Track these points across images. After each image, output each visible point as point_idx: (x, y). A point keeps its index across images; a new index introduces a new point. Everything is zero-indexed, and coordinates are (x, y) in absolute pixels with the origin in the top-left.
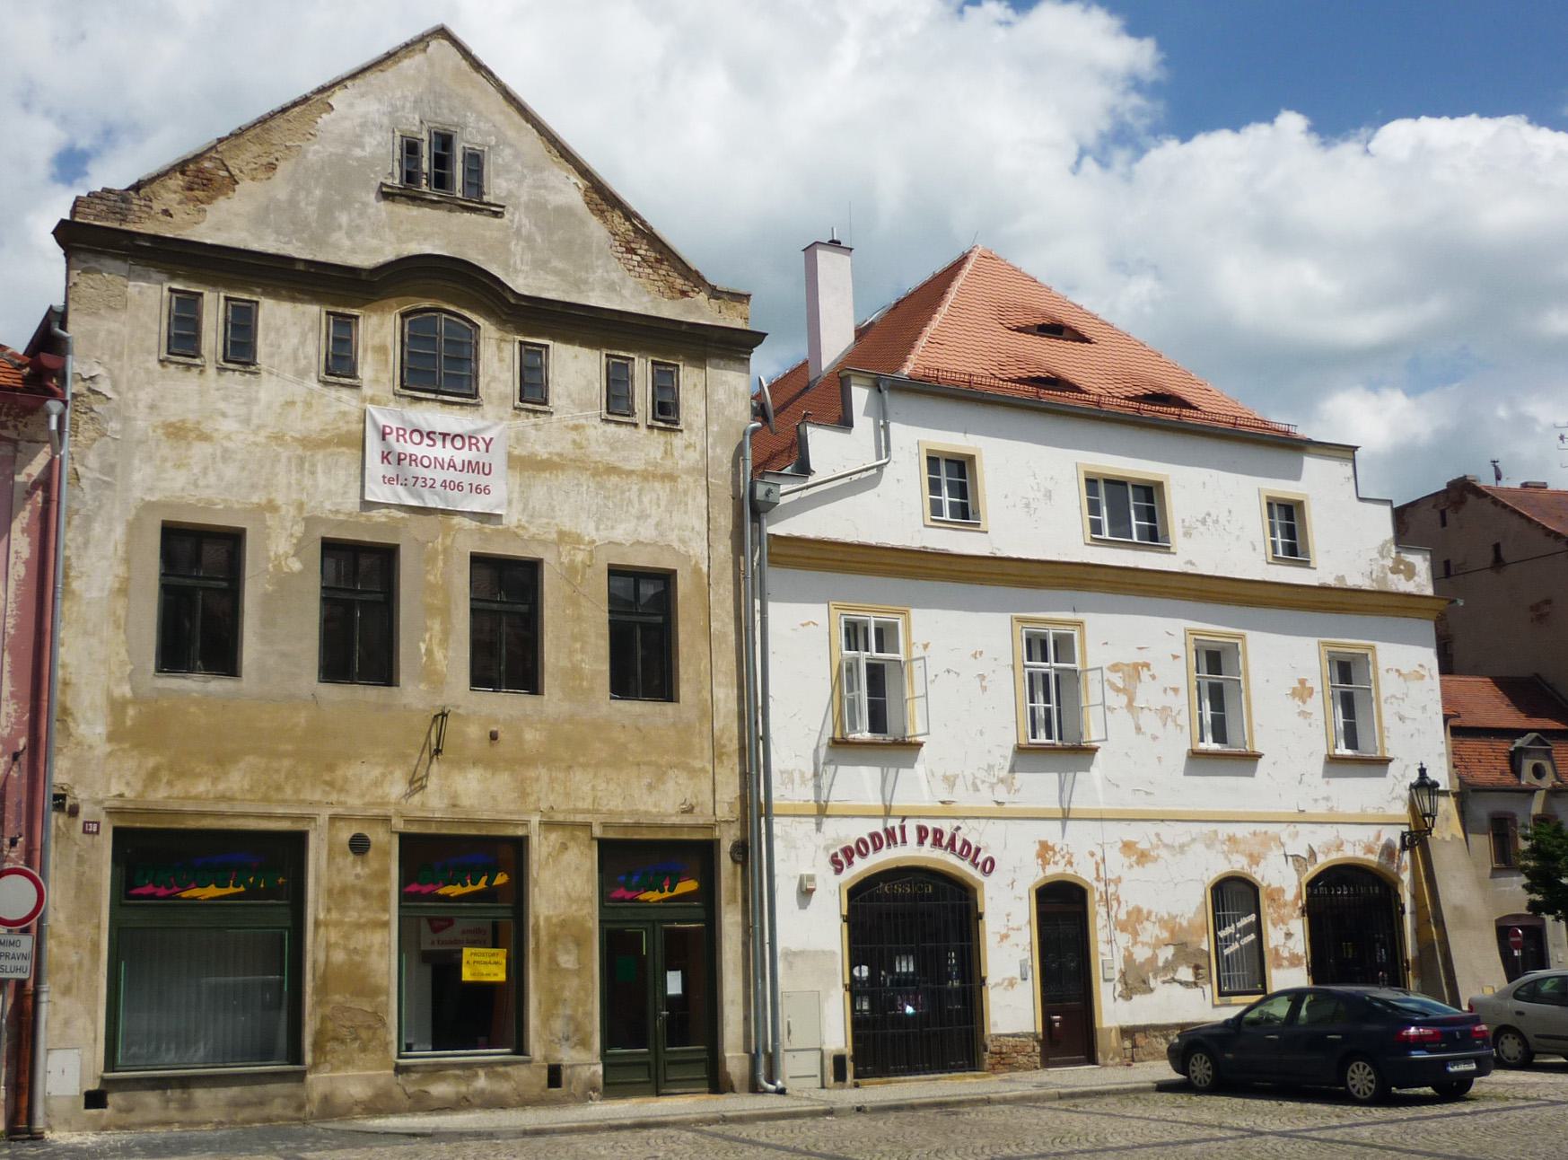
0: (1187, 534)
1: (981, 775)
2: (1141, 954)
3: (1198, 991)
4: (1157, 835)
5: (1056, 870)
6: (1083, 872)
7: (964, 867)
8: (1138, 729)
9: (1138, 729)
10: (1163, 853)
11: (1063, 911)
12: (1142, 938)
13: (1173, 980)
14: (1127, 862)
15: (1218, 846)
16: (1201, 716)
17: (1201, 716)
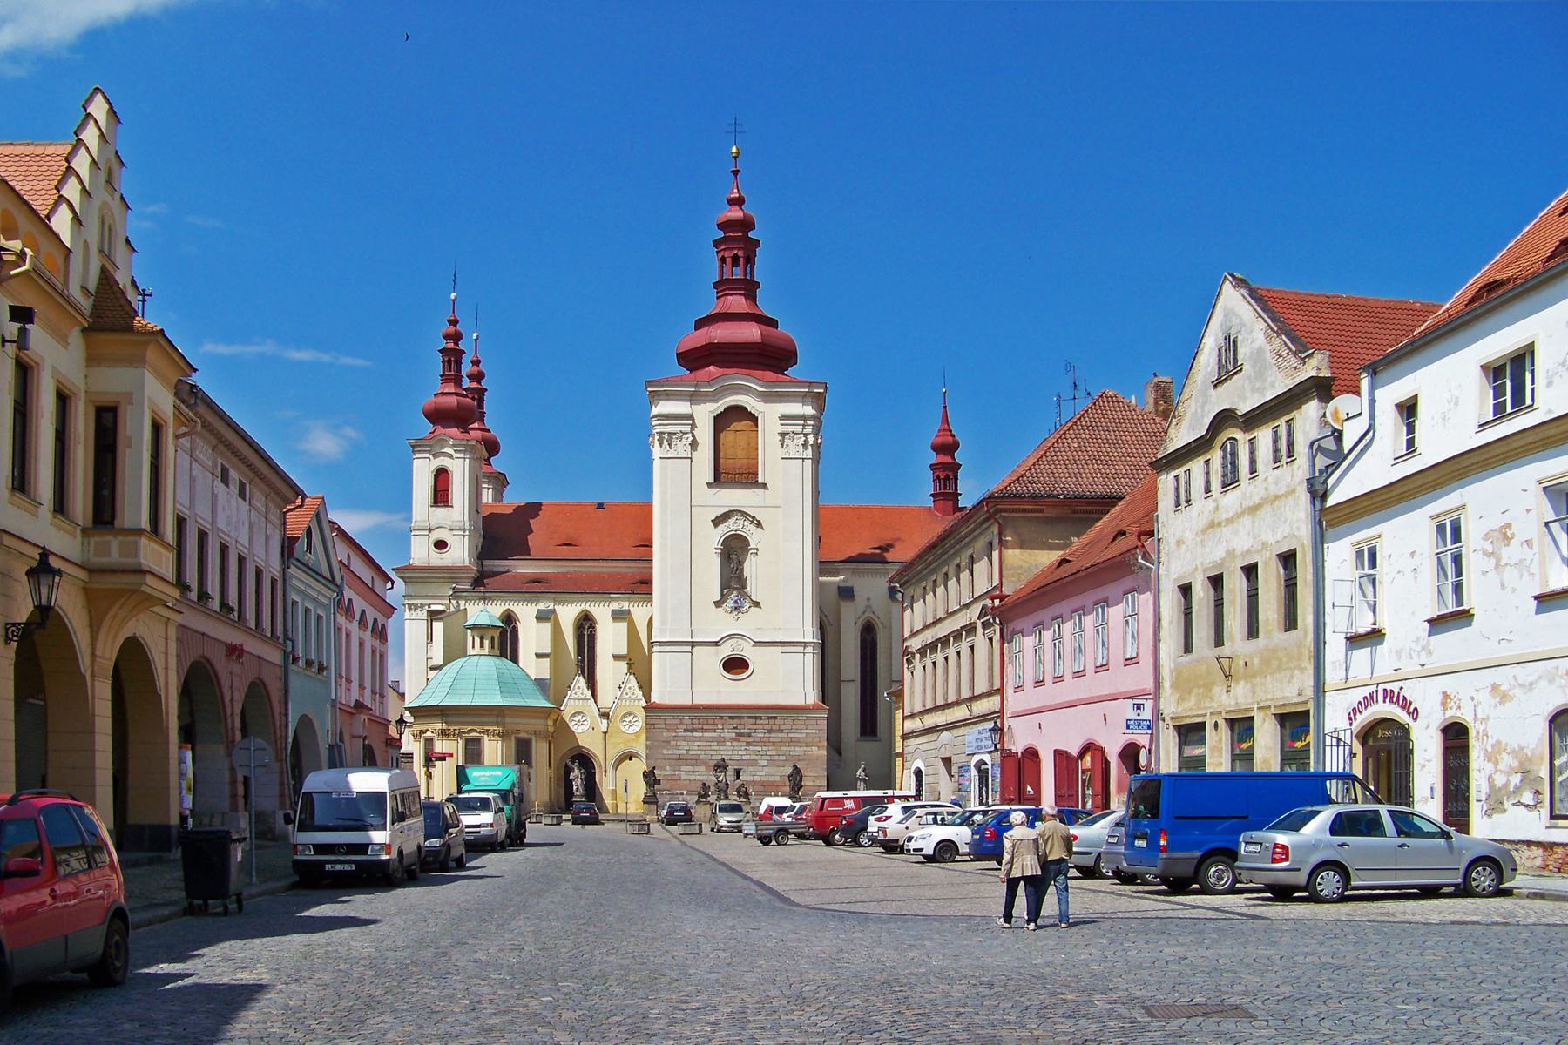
0: (1550, 384)
1: (1413, 646)
2: (1500, 780)
3: (1535, 813)
4: (1515, 678)
5: (1452, 714)
6: (1466, 716)
7: (1403, 717)
8: (1503, 586)
9: (1503, 586)
10: (1517, 692)
11: (1455, 737)
12: (1502, 766)
13: (1519, 803)
14: (1493, 702)
15: (1558, 681)
16: (1177, 489)
17: (1177, 489)
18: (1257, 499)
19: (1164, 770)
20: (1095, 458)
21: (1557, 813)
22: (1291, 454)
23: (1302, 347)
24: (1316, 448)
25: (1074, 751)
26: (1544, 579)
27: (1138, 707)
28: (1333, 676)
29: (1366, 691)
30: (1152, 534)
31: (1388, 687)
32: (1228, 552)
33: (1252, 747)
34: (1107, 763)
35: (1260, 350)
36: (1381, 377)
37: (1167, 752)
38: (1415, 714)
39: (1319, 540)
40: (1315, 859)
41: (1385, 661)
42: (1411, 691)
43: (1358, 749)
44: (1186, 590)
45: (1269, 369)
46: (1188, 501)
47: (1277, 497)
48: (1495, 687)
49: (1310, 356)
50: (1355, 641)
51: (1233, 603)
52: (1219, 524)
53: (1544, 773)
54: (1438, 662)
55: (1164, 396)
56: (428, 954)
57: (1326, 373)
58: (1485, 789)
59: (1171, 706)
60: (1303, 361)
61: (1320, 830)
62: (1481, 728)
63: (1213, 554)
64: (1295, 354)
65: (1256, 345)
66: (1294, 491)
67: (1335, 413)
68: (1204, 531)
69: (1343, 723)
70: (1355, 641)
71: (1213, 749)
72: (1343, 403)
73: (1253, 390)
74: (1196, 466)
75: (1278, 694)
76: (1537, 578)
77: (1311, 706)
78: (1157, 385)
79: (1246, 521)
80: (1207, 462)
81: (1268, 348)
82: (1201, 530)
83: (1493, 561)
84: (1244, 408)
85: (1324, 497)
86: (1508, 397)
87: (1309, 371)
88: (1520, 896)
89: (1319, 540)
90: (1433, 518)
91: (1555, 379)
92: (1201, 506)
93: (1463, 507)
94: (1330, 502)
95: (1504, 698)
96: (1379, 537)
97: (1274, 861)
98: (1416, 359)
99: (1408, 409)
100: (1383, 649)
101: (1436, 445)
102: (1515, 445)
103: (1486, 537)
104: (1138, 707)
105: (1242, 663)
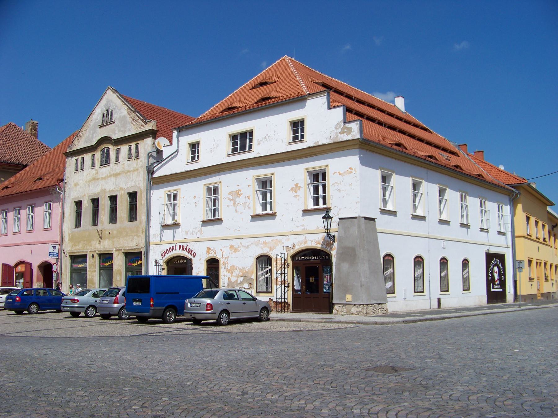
0: (259, 144)
2: (233, 279)
5: (212, 255)
6: (218, 256)
8: (236, 211)
9: (236, 211)
10: (242, 248)
12: (234, 274)
14: (231, 252)
18: (118, 171)
19: (151, 273)
20: (10, 148)
21: (258, 291)
22: (137, 156)
23: (145, 120)
24: (150, 155)
25: (12, 264)
26: (255, 209)
27: (54, 247)
28: (153, 239)
29: (171, 246)
30: (62, 180)
31: (182, 244)
32: (102, 190)
33: (112, 264)
34: (32, 270)
35: (124, 116)
36: (182, 133)
37: (66, 266)
38: (194, 255)
39: (149, 190)
40: (221, 309)
41: (180, 235)
42: (191, 246)
43: (165, 267)
44: (79, 204)
45: (126, 123)
46: (82, 169)
47: (129, 171)
48: (232, 247)
49: (150, 122)
50: (165, 227)
51: (104, 209)
52: (98, 179)
53: (254, 277)
54: (205, 236)
55: (35, 128)
56: (42, 368)
57: (155, 129)
58: (227, 282)
59: (68, 247)
60: (146, 123)
61: (220, 298)
62: (225, 261)
63: (94, 190)
64: (142, 120)
65: (123, 114)
66: (137, 170)
67: (159, 143)
68: (90, 181)
69: (159, 257)
70: (165, 227)
71: (91, 265)
72: (162, 141)
73: (120, 131)
74: (88, 157)
75: (126, 245)
76: (252, 209)
77: (143, 251)
78: (33, 123)
79: (113, 179)
80: (93, 155)
81: (128, 116)
82: (83, 181)
83: (232, 202)
84: (114, 137)
85: (153, 173)
86: (239, 146)
87: (148, 127)
88: (273, 320)
89: (149, 190)
90: (205, 185)
91: (261, 143)
92: (88, 172)
93: (220, 182)
94: (155, 175)
95: (236, 250)
96: (179, 190)
97: (207, 310)
98: (198, 129)
99: (194, 146)
100: (179, 231)
101: (207, 159)
102: (245, 163)
103: (230, 193)
104: (54, 247)
105: (107, 233)
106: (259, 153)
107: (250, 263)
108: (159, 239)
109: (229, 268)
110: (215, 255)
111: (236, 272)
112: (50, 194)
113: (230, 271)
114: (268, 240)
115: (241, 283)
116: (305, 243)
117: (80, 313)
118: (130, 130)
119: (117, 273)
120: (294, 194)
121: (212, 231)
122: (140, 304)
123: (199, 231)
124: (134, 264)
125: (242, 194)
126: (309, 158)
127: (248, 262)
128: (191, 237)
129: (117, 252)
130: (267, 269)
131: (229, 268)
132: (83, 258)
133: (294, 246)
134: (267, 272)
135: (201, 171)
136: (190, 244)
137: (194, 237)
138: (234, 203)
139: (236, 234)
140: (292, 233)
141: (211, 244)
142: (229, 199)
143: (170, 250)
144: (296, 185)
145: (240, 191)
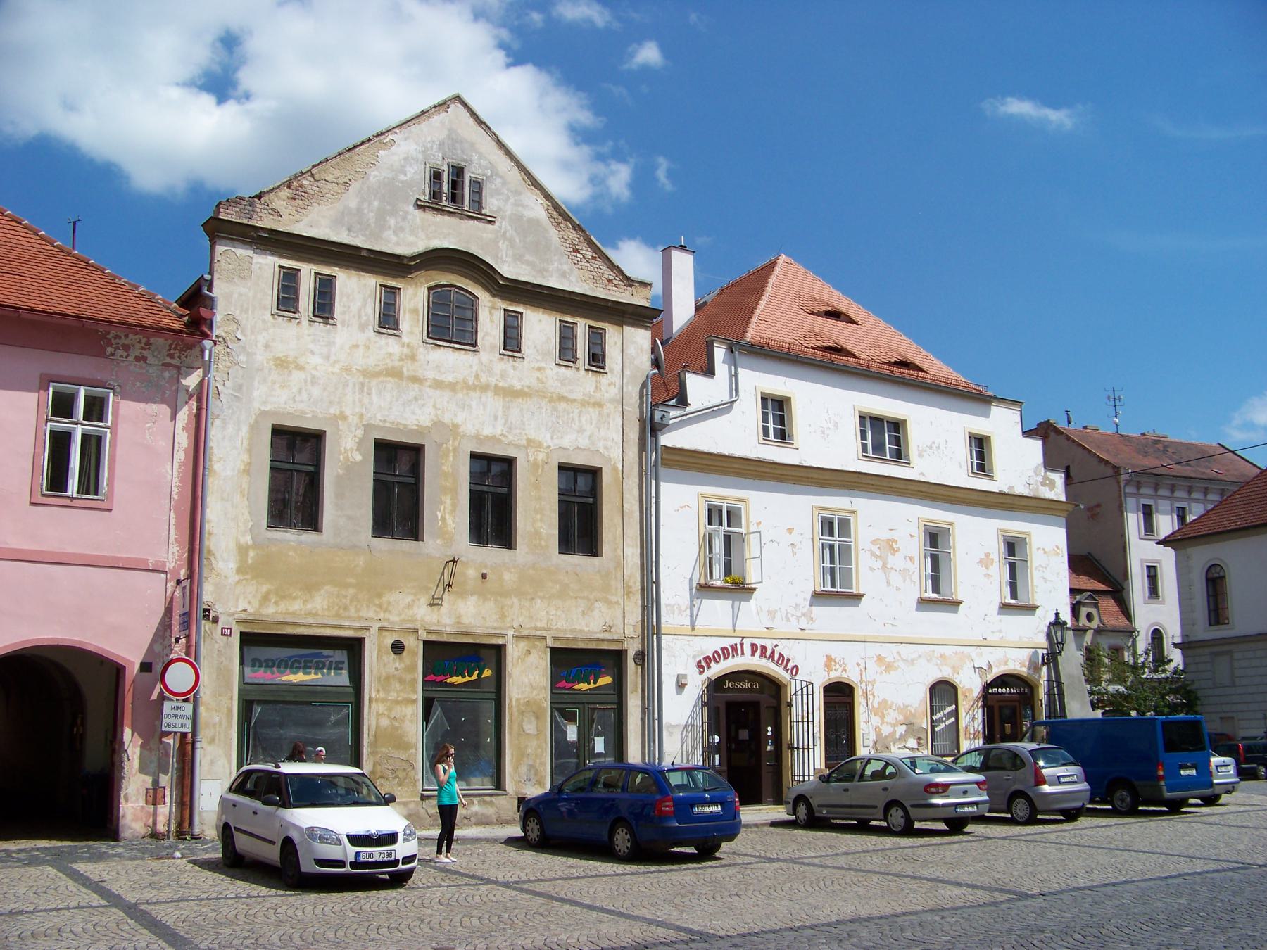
0: (920, 455)
2: (886, 730)
5: (836, 675)
6: (852, 676)
8: (888, 583)
9: (888, 583)
10: (901, 664)
31: (759, 642)
41: (750, 618)
42: (785, 649)
48: (880, 659)
50: (705, 589)
77: (632, 648)
83: (880, 563)
84: (508, 270)
94: (667, 440)
95: (889, 667)
100: (749, 608)
103: (874, 542)
106: (922, 474)
107: (918, 698)
108: (687, 621)
109: (876, 705)
110: (844, 675)
111: (892, 715)
112: (101, 354)
113: (881, 711)
114: (948, 651)
115: (903, 738)
116: (1006, 663)
117: (1187, 799)
118: (563, 275)
119: (522, 713)
120: (984, 571)
121: (833, 617)
122: (1194, 772)
123: (803, 615)
124: (583, 686)
125: (898, 549)
126: (1040, 516)
127: (912, 696)
128: (782, 628)
129: (523, 645)
130: (948, 710)
131: (876, 705)
132: (487, 655)
133: (990, 666)
134: (949, 716)
135: (803, 473)
136: (782, 644)
137: (792, 628)
138: (884, 566)
139: (888, 633)
140: (984, 643)
141: (835, 650)
142: (873, 554)
143: (726, 653)
144: (988, 555)
145: (896, 541)
